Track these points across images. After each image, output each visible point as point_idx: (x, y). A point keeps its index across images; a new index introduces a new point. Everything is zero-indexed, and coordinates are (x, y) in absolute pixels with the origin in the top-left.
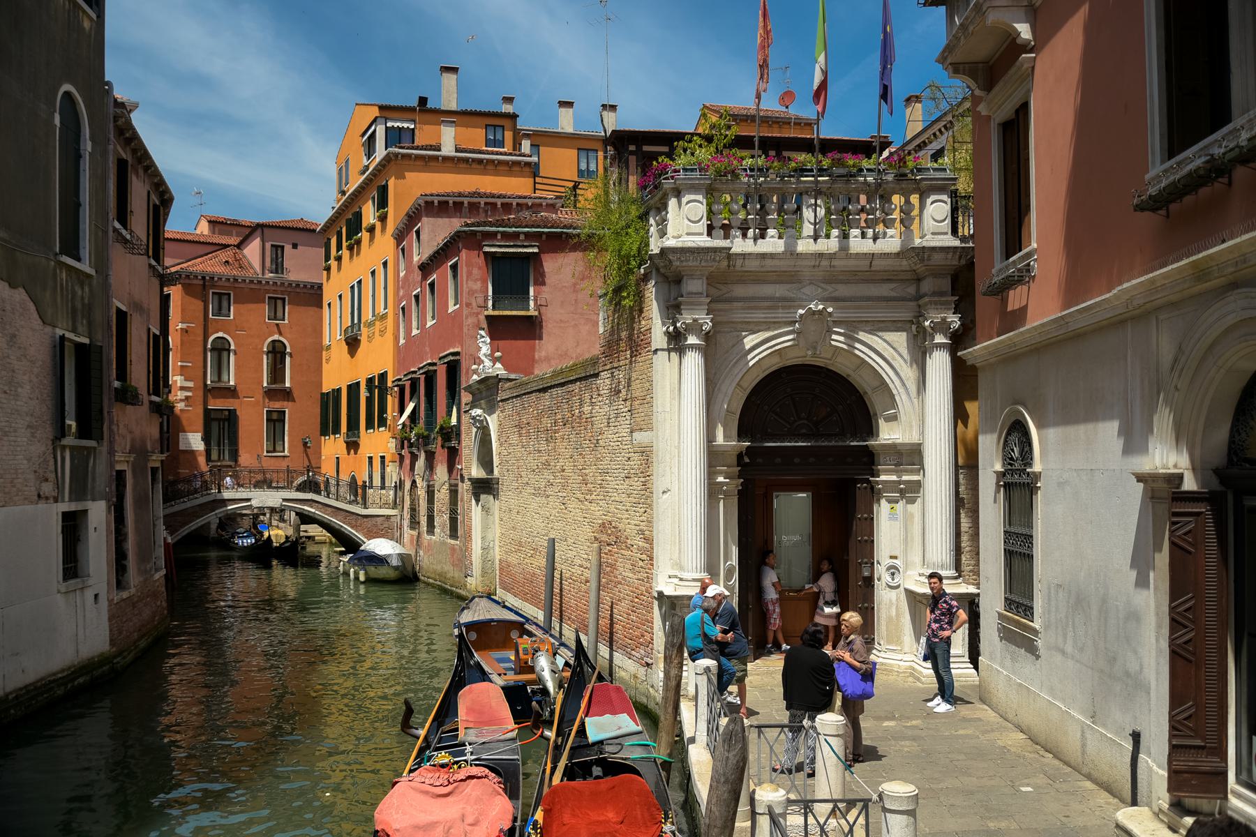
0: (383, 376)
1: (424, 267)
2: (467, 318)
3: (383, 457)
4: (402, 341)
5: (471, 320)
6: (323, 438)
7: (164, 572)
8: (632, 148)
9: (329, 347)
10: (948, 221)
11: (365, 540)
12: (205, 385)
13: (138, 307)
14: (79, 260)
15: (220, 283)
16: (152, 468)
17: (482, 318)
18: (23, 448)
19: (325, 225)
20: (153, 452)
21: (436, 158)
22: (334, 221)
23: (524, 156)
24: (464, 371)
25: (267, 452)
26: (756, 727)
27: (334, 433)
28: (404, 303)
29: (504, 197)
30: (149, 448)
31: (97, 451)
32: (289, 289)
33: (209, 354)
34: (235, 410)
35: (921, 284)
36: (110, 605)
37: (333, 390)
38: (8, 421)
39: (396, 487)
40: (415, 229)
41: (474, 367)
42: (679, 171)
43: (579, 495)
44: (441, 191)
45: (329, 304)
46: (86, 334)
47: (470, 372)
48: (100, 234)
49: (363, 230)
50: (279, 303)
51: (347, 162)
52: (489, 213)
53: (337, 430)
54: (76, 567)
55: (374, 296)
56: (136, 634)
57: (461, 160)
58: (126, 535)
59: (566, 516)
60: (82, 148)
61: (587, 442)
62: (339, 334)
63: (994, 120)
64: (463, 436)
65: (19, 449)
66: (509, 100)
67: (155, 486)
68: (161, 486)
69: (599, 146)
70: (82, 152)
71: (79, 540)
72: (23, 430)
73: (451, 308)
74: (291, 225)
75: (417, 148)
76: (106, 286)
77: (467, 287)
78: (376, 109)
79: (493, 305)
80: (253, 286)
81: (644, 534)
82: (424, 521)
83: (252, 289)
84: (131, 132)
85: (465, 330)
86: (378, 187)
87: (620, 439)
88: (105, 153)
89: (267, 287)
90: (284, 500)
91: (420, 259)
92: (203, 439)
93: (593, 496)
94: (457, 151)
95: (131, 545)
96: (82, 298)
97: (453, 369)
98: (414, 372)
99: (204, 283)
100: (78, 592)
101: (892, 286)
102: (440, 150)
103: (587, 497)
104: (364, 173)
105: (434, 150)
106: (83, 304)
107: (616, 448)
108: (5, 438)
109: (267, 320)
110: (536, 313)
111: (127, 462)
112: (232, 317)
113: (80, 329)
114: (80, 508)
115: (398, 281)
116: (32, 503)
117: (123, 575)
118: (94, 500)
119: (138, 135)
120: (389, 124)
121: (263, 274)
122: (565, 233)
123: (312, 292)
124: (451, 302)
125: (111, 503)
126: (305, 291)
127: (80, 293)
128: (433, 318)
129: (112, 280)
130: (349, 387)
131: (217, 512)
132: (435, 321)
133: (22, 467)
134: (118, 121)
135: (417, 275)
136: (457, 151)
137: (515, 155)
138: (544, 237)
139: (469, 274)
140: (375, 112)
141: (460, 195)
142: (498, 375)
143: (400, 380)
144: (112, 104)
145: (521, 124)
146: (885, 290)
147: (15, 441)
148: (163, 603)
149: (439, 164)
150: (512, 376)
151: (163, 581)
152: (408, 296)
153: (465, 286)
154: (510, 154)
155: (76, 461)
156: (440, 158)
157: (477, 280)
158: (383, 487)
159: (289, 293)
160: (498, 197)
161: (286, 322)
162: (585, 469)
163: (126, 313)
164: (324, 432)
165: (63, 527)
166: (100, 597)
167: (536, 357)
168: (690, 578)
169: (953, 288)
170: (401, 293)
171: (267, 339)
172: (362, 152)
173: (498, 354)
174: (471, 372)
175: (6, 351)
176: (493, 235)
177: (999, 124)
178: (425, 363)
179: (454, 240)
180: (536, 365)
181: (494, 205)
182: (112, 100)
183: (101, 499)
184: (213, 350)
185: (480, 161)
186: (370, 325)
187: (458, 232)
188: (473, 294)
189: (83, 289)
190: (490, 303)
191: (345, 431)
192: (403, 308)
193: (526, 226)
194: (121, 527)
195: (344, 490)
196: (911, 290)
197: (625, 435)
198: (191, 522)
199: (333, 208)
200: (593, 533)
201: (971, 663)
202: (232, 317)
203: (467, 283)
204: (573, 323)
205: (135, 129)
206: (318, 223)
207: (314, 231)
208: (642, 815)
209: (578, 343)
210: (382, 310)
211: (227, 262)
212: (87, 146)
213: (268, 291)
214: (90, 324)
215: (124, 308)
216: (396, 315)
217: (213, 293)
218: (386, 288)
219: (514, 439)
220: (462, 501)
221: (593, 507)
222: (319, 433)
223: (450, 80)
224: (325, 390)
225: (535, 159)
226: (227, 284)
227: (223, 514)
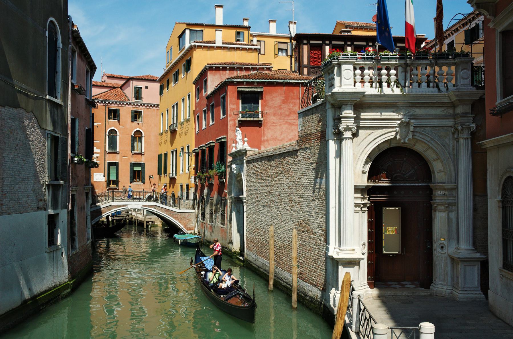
1: (209, 97)
2: (230, 121)
3: (187, 186)
7: (90, 241)
8: (305, 42)
10: (470, 78)
14: (56, 98)
18: (31, 186)
19: (161, 78)
21: (212, 47)
22: (165, 76)
23: (254, 45)
26: (390, 329)
28: (199, 114)
34: (118, 163)
35: (456, 108)
38: (24, 174)
40: (204, 80)
42: (348, 56)
43: (288, 207)
44: (217, 62)
51: (171, 49)
55: (184, 110)
58: (75, 224)
59: (281, 217)
61: (292, 182)
63: (497, 30)
65: (29, 186)
67: (87, 200)
69: (288, 41)
72: (31, 178)
73: (222, 117)
75: (204, 42)
77: (230, 107)
78: (186, 25)
81: (321, 228)
84: (79, 39)
87: (309, 182)
90: (143, 205)
93: (295, 208)
94: (223, 44)
97: (223, 145)
100: (54, 252)
101: (442, 109)
102: (214, 43)
103: (292, 209)
105: (212, 43)
107: (307, 186)
108: (23, 182)
116: (35, 211)
117: (73, 243)
122: (276, 82)
133: (31, 194)
136: (223, 44)
137: (250, 45)
138: (266, 83)
141: (225, 64)
146: (438, 111)
147: (28, 183)
148: (91, 255)
151: (90, 245)
154: (247, 45)
156: (215, 47)
162: (291, 195)
165: (48, 221)
167: (262, 140)
168: (346, 249)
169: (472, 112)
173: (246, 139)
174: (231, 147)
175: (24, 141)
177: (500, 32)
179: (224, 85)
180: (262, 144)
186: (182, 124)
187: (225, 82)
192: (198, 116)
194: (73, 220)
196: (451, 111)
197: (312, 180)
200: (295, 226)
201: (482, 291)
204: (280, 123)
205: (81, 37)
206: (157, 77)
208: (16, 167)
209: (282, 133)
211: (116, 95)
212: (60, 45)
221: (295, 214)
223: (219, 11)
225: (258, 47)
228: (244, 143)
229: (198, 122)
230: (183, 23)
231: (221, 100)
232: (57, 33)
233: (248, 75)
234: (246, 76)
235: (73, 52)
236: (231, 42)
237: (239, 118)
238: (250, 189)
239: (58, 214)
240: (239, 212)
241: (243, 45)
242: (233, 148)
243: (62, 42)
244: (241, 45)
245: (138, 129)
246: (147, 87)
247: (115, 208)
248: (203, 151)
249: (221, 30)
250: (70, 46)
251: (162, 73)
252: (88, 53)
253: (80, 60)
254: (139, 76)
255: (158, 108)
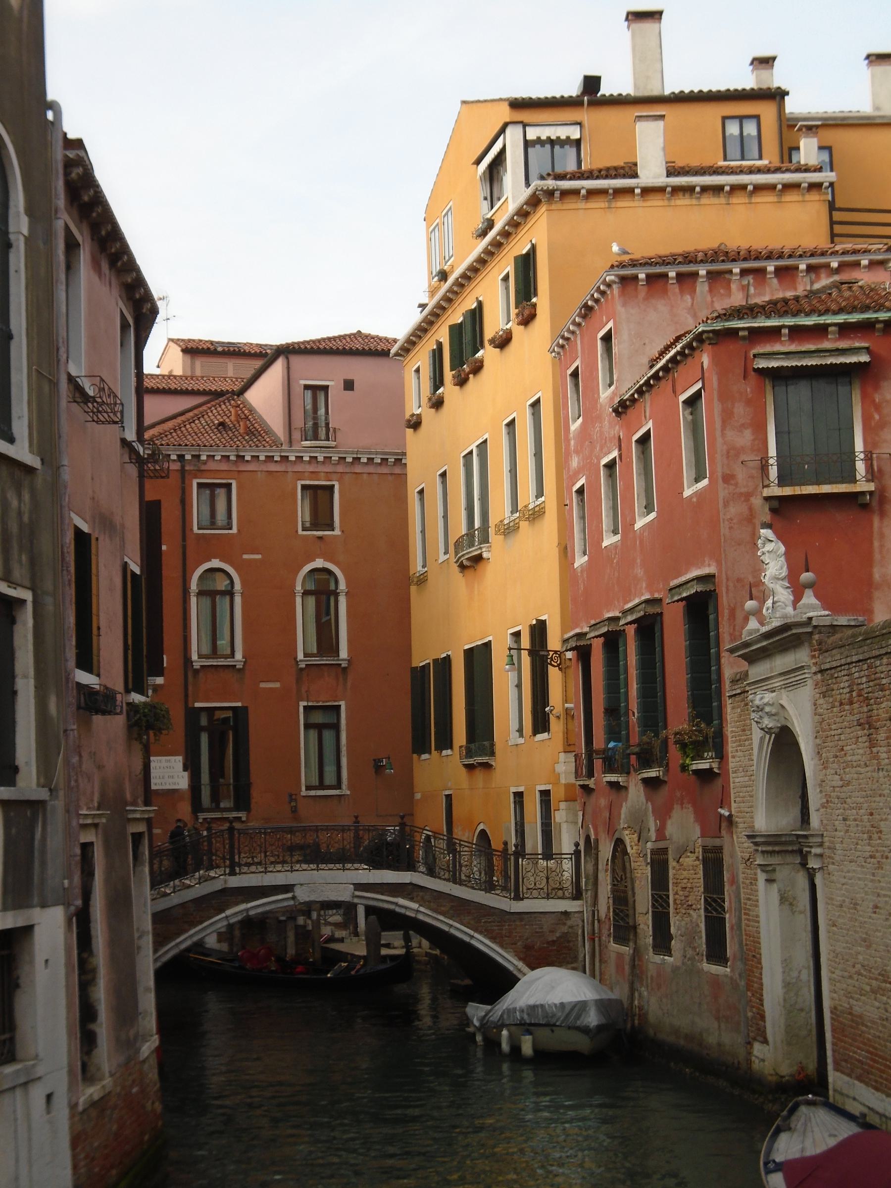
0: (539, 630)
2: (726, 504)
3: (545, 794)
4: (580, 561)
5: (736, 510)
6: (415, 756)
9: (422, 580)
11: (525, 969)
12: (188, 661)
13: (106, 522)
15: (212, 466)
16: (133, 834)
17: (757, 502)
20: (134, 803)
21: (630, 191)
23: (807, 169)
24: (725, 613)
25: (308, 788)
27: (440, 748)
29: (812, 255)
30: (128, 796)
31: (49, 808)
32: (340, 469)
33: (193, 600)
36: (72, 1116)
37: (436, 661)
39: (577, 853)
40: (601, 334)
41: (750, 604)
44: (679, 248)
45: (421, 492)
46: (27, 583)
47: (740, 618)
48: (46, 388)
49: (486, 343)
50: (221, 493)
52: (752, 290)
53: (445, 741)
54: (12, 1040)
56: (114, 1172)
57: (677, 190)
58: (94, 971)
60: (11, 229)
62: (442, 550)
64: (731, 747)
66: (765, 62)
68: (147, 870)
70: (12, 237)
71: (18, 986)
74: (340, 345)
75: (590, 175)
76: (56, 487)
78: (505, 108)
79: (780, 477)
80: (273, 467)
82: (645, 924)
83: (270, 472)
84: (92, 192)
85: (724, 530)
86: (516, 258)
88: (49, 235)
89: (299, 468)
90: (359, 887)
91: (614, 394)
92: (185, 769)
94: (669, 174)
95: (101, 994)
96: (20, 514)
98: (616, 619)
99: (183, 467)
102: (635, 175)
104: (483, 234)
105: (624, 176)
106: (21, 525)
109: (300, 532)
110: (871, 487)
111: (96, 825)
112: (235, 530)
113: (18, 573)
114: (20, 923)
115: (568, 440)
118: (44, 905)
119: (104, 196)
120: (532, 133)
121: (290, 442)
123: (384, 470)
124: (687, 473)
125: (72, 909)
126: (371, 469)
127: (15, 503)
128: (649, 508)
129: (66, 475)
130: (469, 654)
131: (229, 912)
132: (653, 515)
134: (70, 173)
135: (610, 426)
136: (669, 174)
137: (788, 170)
139: (727, 416)
140: (505, 113)
142: (810, 619)
143: (580, 636)
144: (60, 143)
145: (793, 106)
149: (636, 204)
150: (842, 620)
151: (153, 1061)
152: (589, 467)
153: (719, 440)
154: (777, 170)
155: (14, 831)
157: (743, 426)
158: (548, 855)
159: (341, 476)
160: (769, 257)
161: (337, 532)
163: (89, 535)
164: (420, 745)
166: (55, 1099)
167: (877, 576)
170: (575, 462)
171: (301, 567)
172: (481, 190)
173: (806, 576)
174: (739, 615)
176: (774, 333)
178: (637, 601)
181: (762, 271)
182: (61, 137)
183: (55, 904)
184: (200, 594)
185: (717, 190)
188: (737, 455)
189: (20, 500)
190: (773, 472)
191: (463, 741)
193: (840, 311)
195: (475, 867)
198: (179, 934)
199: (423, 306)
202: (235, 530)
203: (723, 435)
205: (98, 186)
207: (385, 354)
210: (532, 498)
211: (222, 424)
213: (300, 475)
214: (33, 563)
215: (85, 528)
216: (563, 505)
217: (199, 485)
218: (538, 455)
219: (857, 752)
220: (733, 881)
222: (411, 752)
224: (418, 661)
226: (224, 466)
227: (239, 918)
228: (798, 597)
229: (582, 518)
230: (501, 100)
231: (683, 415)
232: (9, 173)
233: (797, 299)
234: (785, 301)
235: (72, 246)
236: (707, 162)
237: (768, 486)
238: (843, 795)
239: (28, 930)
240: (791, 904)
241: (759, 171)
242: (746, 619)
243: (30, 211)
244: (751, 171)
245: (319, 563)
246: (349, 385)
247: (243, 902)
248: (613, 641)
249: (662, 117)
250: (59, 225)
251: (415, 317)
252: (125, 250)
253: (95, 278)
254: (837, 109)
255: (397, 470)
